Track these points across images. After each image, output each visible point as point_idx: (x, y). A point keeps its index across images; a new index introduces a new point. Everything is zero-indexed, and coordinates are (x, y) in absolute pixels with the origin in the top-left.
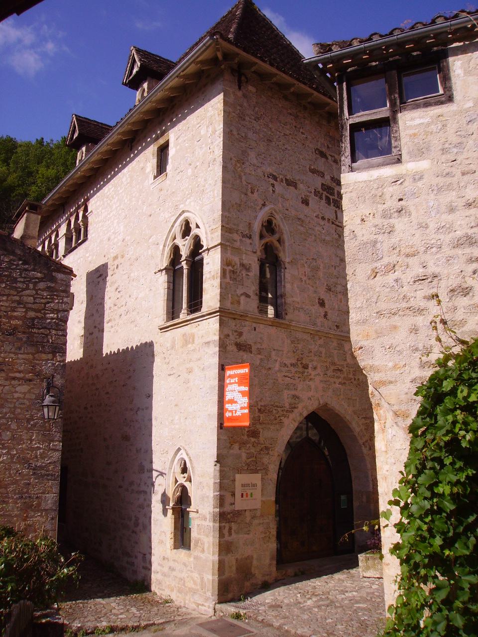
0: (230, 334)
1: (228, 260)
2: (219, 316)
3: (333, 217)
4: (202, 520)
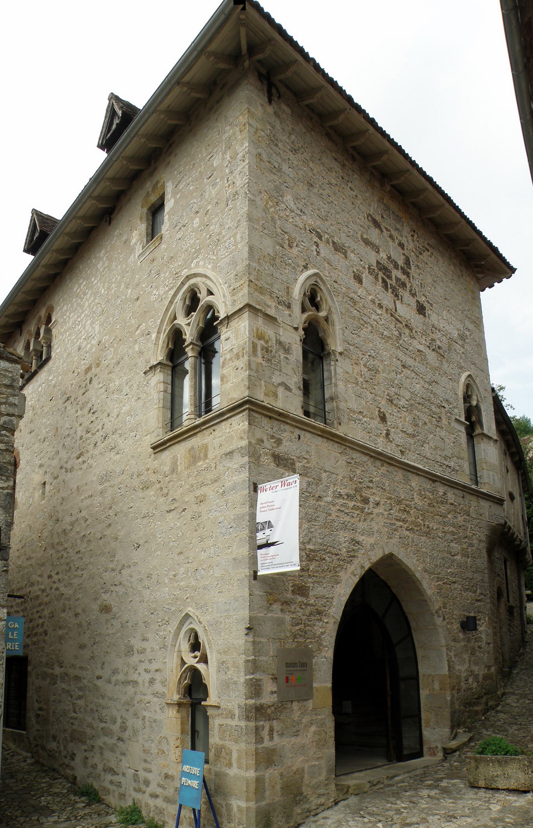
0: (265, 439)
1: (260, 332)
2: (247, 411)
3: (391, 306)
4: (226, 718)
